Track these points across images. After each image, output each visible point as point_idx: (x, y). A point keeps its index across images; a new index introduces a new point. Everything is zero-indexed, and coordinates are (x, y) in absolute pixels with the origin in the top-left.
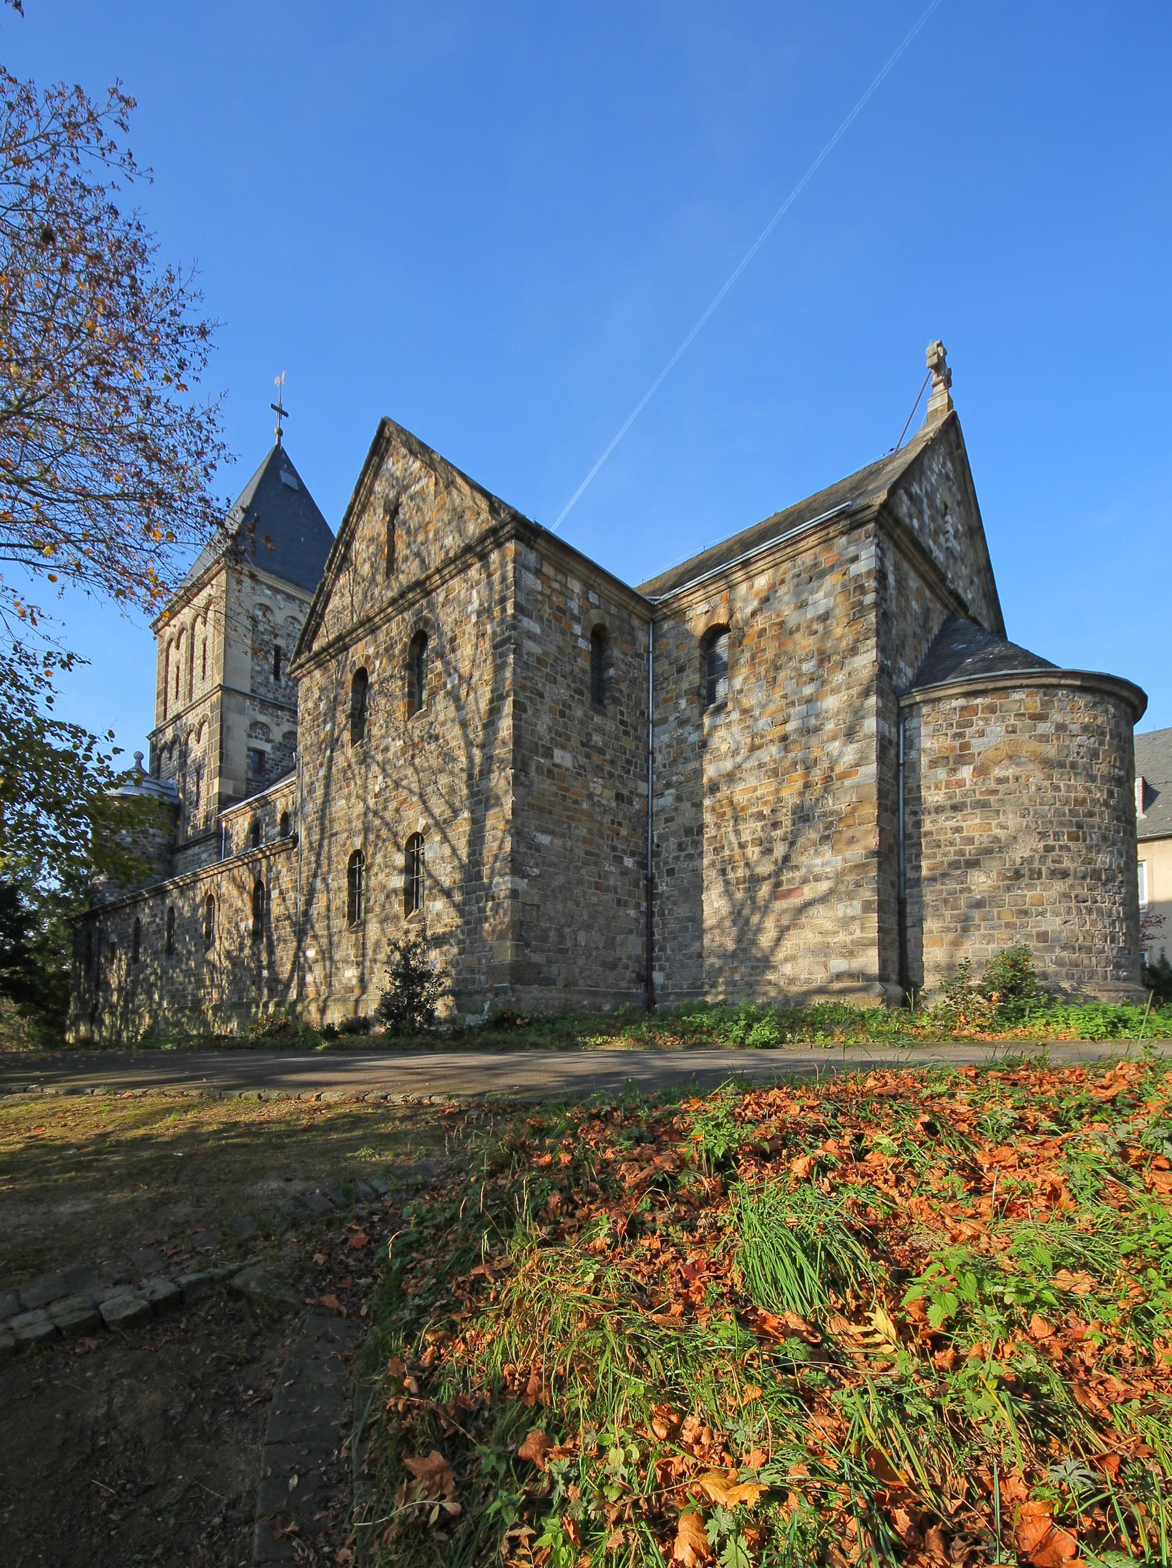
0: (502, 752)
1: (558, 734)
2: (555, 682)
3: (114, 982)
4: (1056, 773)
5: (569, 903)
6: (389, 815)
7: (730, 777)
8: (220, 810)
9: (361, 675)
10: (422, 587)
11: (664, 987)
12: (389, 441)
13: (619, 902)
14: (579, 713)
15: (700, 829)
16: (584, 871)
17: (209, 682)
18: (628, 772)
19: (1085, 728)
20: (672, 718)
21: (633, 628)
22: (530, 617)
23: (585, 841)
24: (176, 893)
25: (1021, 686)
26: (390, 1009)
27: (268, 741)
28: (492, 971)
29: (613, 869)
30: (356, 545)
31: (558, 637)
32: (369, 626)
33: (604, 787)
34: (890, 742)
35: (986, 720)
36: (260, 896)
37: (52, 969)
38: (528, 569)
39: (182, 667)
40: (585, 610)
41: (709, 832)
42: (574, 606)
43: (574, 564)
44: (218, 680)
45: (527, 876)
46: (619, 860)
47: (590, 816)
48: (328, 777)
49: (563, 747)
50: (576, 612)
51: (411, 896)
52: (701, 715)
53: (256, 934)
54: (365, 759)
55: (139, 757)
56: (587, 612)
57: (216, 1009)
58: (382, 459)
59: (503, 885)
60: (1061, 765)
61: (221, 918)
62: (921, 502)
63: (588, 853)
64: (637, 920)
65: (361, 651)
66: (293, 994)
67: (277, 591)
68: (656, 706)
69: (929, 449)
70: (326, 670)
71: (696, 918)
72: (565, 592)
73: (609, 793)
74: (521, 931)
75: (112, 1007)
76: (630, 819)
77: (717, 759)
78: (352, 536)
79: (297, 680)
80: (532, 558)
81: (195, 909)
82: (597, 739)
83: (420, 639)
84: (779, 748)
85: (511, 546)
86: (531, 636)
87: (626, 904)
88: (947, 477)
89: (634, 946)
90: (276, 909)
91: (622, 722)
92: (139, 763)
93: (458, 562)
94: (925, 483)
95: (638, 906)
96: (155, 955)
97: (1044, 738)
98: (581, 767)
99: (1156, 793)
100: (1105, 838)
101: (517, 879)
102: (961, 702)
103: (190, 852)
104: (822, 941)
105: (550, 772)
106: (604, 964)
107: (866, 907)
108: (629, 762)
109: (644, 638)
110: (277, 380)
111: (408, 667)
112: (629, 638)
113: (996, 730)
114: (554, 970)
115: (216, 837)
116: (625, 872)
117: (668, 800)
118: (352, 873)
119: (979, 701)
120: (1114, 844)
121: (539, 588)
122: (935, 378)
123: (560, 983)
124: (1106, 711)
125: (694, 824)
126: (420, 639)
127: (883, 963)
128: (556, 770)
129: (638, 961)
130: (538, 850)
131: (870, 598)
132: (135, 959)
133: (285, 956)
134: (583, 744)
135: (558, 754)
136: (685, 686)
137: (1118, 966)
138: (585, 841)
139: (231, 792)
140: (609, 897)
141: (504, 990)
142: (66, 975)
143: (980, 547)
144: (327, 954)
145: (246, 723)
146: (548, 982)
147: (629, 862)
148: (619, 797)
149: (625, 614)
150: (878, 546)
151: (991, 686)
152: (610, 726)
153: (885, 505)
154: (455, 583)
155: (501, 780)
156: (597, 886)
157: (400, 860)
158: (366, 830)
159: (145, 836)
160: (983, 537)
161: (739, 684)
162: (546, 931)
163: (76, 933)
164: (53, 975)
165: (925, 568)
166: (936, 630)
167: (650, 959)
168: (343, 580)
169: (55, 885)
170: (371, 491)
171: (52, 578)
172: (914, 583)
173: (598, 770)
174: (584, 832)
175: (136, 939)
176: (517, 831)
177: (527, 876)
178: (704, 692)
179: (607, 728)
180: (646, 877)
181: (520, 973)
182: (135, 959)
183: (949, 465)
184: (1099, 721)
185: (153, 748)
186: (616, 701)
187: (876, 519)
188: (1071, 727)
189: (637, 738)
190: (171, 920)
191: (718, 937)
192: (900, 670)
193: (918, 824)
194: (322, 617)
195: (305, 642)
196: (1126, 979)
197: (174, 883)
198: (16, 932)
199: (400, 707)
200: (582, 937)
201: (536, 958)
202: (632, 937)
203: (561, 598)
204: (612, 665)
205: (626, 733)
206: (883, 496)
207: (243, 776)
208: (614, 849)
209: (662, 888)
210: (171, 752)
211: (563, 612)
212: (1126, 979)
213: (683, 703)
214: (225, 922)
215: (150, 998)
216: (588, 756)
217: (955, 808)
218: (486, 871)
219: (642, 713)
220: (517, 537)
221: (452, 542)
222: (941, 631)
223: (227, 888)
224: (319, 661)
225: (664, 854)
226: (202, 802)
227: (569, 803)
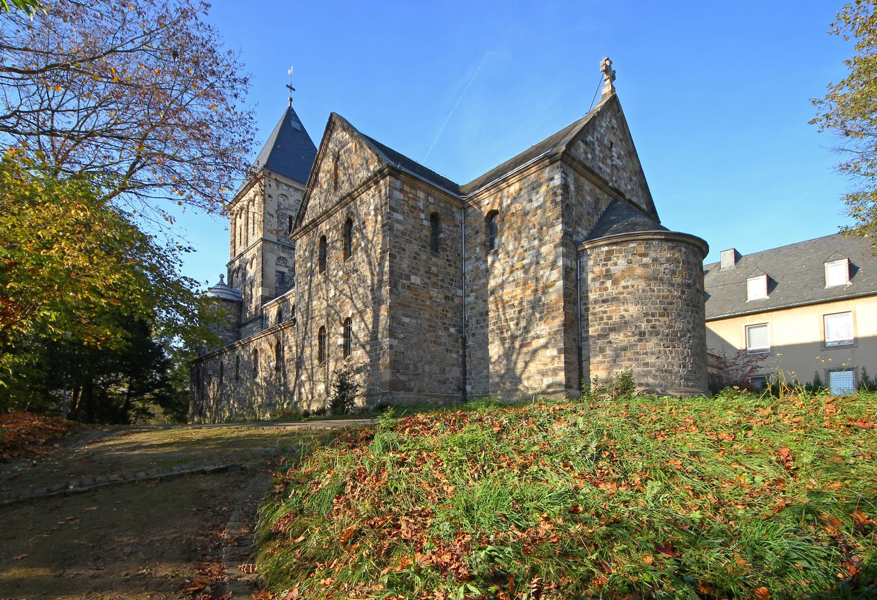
0: (386, 278)
2: (411, 242)
3: (211, 395)
4: (652, 283)
5: (420, 351)
6: (338, 308)
7: (502, 286)
8: (262, 304)
9: (323, 239)
10: (351, 196)
11: (471, 393)
12: (334, 123)
13: (447, 350)
14: (424, 257)
15: (487, 313)
16: (427, 335)
17: (256, 236)
18: (451, 285)
19: (668, 260)
22: (397, 212)
23: (428, 320)
24: (240, 348)
26: (336, 404)
27: (286, 267)
28: (382, 384)
30: (321, 175)
31: (412, 221)
32: (327, 214)
34: (572, 269)
35: (618, 257)
36: (279, 349)
37: (179, 390)
38: (396, 189)
39: (243, 228)
41: (491, 314)
42: (421, 205)
43: (419, 184)
44: (261, 235)
45: (398, 338)
46: (447, 329)
47: (431, 308)
48: (310, 289)
49: (416, 275)
50: (422, 207)
51: (347, 348)
52: (486, 256)
53: (277, 369)
54: (327, 279)
55: (222, 277)
57: (260, 407)
58: (332, 132)
59: (386, 342)
60: (655, 279)
61: (262, 360)
62: (594, 144)
63: (429, 326)
64: (457, 359)
65: (324, 227)
66: (295, 398)
67: (290, 187)
68: (466, 251)
69: (600, 114)
70: (309, 235)
71: (486, 359)
72: (416, 198)
73: (441, 296)
74: (394, 365)
75: (210, 408)
77: (494, 277)
78: (319, 170)
79: (295, 241)
80: (398, 184)
81: (249, 357)
82: (434, 269)
83: (349, 222)
84: (519, 273)
85: (388, 178)
86: (398, 222)
87: (451, 351)
88: (613, 128)
89: (456, 372)
90: (287, 356)
91: (447, 260)
92: (222, 280)
93: (366, 185)
94: (596, 134)
95: (458, 352)
96: (230, 380)
97: (645, 265)
98: (425, 284)
99: (776, 284)
100: (679, 315)
101: (393, 340)
102: (606, 248)
103: (248, 327)
104: (543, 369)
105: (409, 287)
106: (439, 381)
107: (560, 352)
108: (452, 280)
109: (458, 217)
110: (289, 72)
111: (345, 235)
113: (622, 263)
114: (412, 384)
115: (261, 318)
116: (450, 335)
117: (471, 299)
118: (321, 338)
119: (614, 247)
120: (685, 318)
122: (606, 77)
123: (415, 391)
124: (680, 251)
125: (484, 311)
126: (349, 222)
127: (568, 379)
130: (403, 325)
131: (559, 199)
132: (221, 383)
133: (292, 377)
134: (426, 272)
136: (479, 241)
137: (687, 380)
138: (428, 320)
141: (386, 394)
142: (187, 393)
144: (310, 378)
145: (275, 258)
146: (410, 390)
147: (452, 330)
148: (446, 298)
149: (449, 206)
150: (563, 172)
151: (619, 240)
152: (441, 262)
153: (564, 153)
154: (364, 196)
155: (385, 290)
156: (435, 342)
157: (342, 330)
158: (328, 315)
159: (227, 317)
161: (506, 239)
162: (408, 365)
163: (192, 370)
164: (181, 393)
165: (594, 178)
166: (604, 209)
167: (465, 379)
168: (315, 191)
169: (181, 345)
170: (327, 146)
171: (180, 204)
172: (587, 186)
173: (435, 284)
174: (428, 316)
175: (221, 372)
176: (392, 317)
177: (398, 338)
178: (488, 244)
180: (462, 337)
181: (394, 385)
182: (221, 383)
183: (614, 121)
184: (676, 255)
185: (229, 271)
186: (444, 250)
187: (561, 160)
189: (456, 268)
190: (238, 362)
191: (496, 369)
192: (578, 232)
193: (587, 310)
194: (306, 209)
195: (300, 217)
196: (692, 386)
197: (240, 343)
198: (162, 371)
199: (341, 255)
200: (427, 368)
201: (403, 378)
202: (455, 368)
205: (450, 265)
206: (564, 148)
208: (444, 324)
209: (470, 343)
211: (415, 208)
212: (692, 386)
213: (478, 249)
214: (263, 362)
215: (229, 402)
216: (429, 278)
217: (604, 301)
218: (380, 336)
219: (459, 255)
220: (390, 174)
221: (363, 175)
222: (607, 209)
223: (265, 346)
224: (306, 230)
225: (470, 326)
226: (254, 300)
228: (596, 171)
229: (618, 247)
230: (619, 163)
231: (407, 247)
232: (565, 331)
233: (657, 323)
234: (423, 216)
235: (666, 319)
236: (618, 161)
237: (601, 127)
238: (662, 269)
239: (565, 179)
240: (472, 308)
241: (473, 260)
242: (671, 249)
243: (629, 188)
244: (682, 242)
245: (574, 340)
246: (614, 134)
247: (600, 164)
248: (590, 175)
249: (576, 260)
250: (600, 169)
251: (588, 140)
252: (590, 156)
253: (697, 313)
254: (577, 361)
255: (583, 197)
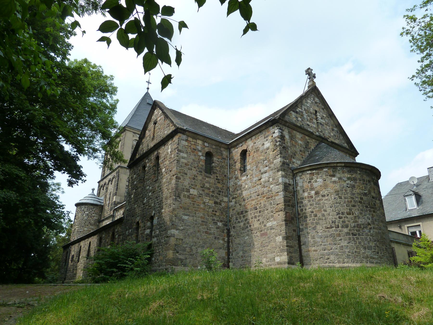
1: (192, 185)
2: (191, 170)
18: (220, 195)
19: (349, 179)
20: (234, 177)
21: (222, 151)
22: (183, 152)
23: (201, 217)
25: (325, 167)
29: (213, 227)
31: (193, 157)
33: (209, 200)
34: (290, 185)
40: (203, 148)
42: (199, 148)
46: (216, 223)
47: (204, 209)
49: (194, 189)
50: (200, 149)
55: (93, 190)
56: (204, 148)
62: (302, 112)
64: (223, 244)
68: (230, 173)
76: (220, 210)
82: (207, 185)
86: (183, 158)
87: (218, 238)
88: (316, 103)
91: (217, 179)
95: (223, 240)
97: (335, 182)
98: (200, 194)
105: (188, 196)
112: (220, 154)
117: (232, 203)
119: (314, 171)
121: (187, 144)
128: (191, 196)
129: (223, 259)
134: (201, 187)
135: (192, 191)
139: (119, 201)
140: (211, 236)
143: (335, 120)
148: (216, 203)
152: (212, 181)
156: (206, 232)
160: (335, 117)
165: (302, 131)
166: (313, 147)
167: (229, 258)
172: (299, 136)
173: (207, 195)
174: (201, 215)
178: (242, 169)
179: (211, 181)
180: (227, 229)
185: (99, 186)
186: (214, 173)
188: (344, 178)
200: (200, 250)
201: (180, 257)
203: (194, 146)
204: (213, 162)
205: (219, 182)
207: (124, 195)
208: (214, 220)
209: (232, 233)
210: (103, 188)
211: (195, 150)
216: (203, 191)
227: (195, 205)
228: (306, 127)
229: (317, 171)
230: (323, 121)
231: (189, 172)
232: (286, 225)
233: (346, 219)
234: (200, 154)
235: (351, 216)
236: (322, 120)
237: (307, 103)
238: (345, 185)
239: (281, 132)
240: (233, 210)
241: (234, 179)
242: (349, 172)
243: (332, 134)
244: (357, 167)
245: (294, 231)
246: (318, 106)
247: (308, 123)
248: (299, 130)
249: (293, 179)
250: (309, 125)
251: (298, 110)
252: (300, 119)
253: (374, 212)
254: (297, 245)
255: (296, 142)
